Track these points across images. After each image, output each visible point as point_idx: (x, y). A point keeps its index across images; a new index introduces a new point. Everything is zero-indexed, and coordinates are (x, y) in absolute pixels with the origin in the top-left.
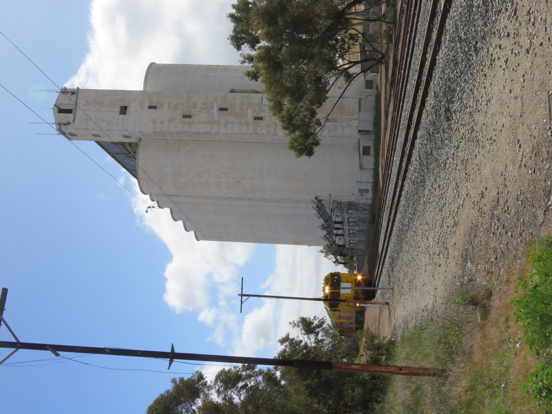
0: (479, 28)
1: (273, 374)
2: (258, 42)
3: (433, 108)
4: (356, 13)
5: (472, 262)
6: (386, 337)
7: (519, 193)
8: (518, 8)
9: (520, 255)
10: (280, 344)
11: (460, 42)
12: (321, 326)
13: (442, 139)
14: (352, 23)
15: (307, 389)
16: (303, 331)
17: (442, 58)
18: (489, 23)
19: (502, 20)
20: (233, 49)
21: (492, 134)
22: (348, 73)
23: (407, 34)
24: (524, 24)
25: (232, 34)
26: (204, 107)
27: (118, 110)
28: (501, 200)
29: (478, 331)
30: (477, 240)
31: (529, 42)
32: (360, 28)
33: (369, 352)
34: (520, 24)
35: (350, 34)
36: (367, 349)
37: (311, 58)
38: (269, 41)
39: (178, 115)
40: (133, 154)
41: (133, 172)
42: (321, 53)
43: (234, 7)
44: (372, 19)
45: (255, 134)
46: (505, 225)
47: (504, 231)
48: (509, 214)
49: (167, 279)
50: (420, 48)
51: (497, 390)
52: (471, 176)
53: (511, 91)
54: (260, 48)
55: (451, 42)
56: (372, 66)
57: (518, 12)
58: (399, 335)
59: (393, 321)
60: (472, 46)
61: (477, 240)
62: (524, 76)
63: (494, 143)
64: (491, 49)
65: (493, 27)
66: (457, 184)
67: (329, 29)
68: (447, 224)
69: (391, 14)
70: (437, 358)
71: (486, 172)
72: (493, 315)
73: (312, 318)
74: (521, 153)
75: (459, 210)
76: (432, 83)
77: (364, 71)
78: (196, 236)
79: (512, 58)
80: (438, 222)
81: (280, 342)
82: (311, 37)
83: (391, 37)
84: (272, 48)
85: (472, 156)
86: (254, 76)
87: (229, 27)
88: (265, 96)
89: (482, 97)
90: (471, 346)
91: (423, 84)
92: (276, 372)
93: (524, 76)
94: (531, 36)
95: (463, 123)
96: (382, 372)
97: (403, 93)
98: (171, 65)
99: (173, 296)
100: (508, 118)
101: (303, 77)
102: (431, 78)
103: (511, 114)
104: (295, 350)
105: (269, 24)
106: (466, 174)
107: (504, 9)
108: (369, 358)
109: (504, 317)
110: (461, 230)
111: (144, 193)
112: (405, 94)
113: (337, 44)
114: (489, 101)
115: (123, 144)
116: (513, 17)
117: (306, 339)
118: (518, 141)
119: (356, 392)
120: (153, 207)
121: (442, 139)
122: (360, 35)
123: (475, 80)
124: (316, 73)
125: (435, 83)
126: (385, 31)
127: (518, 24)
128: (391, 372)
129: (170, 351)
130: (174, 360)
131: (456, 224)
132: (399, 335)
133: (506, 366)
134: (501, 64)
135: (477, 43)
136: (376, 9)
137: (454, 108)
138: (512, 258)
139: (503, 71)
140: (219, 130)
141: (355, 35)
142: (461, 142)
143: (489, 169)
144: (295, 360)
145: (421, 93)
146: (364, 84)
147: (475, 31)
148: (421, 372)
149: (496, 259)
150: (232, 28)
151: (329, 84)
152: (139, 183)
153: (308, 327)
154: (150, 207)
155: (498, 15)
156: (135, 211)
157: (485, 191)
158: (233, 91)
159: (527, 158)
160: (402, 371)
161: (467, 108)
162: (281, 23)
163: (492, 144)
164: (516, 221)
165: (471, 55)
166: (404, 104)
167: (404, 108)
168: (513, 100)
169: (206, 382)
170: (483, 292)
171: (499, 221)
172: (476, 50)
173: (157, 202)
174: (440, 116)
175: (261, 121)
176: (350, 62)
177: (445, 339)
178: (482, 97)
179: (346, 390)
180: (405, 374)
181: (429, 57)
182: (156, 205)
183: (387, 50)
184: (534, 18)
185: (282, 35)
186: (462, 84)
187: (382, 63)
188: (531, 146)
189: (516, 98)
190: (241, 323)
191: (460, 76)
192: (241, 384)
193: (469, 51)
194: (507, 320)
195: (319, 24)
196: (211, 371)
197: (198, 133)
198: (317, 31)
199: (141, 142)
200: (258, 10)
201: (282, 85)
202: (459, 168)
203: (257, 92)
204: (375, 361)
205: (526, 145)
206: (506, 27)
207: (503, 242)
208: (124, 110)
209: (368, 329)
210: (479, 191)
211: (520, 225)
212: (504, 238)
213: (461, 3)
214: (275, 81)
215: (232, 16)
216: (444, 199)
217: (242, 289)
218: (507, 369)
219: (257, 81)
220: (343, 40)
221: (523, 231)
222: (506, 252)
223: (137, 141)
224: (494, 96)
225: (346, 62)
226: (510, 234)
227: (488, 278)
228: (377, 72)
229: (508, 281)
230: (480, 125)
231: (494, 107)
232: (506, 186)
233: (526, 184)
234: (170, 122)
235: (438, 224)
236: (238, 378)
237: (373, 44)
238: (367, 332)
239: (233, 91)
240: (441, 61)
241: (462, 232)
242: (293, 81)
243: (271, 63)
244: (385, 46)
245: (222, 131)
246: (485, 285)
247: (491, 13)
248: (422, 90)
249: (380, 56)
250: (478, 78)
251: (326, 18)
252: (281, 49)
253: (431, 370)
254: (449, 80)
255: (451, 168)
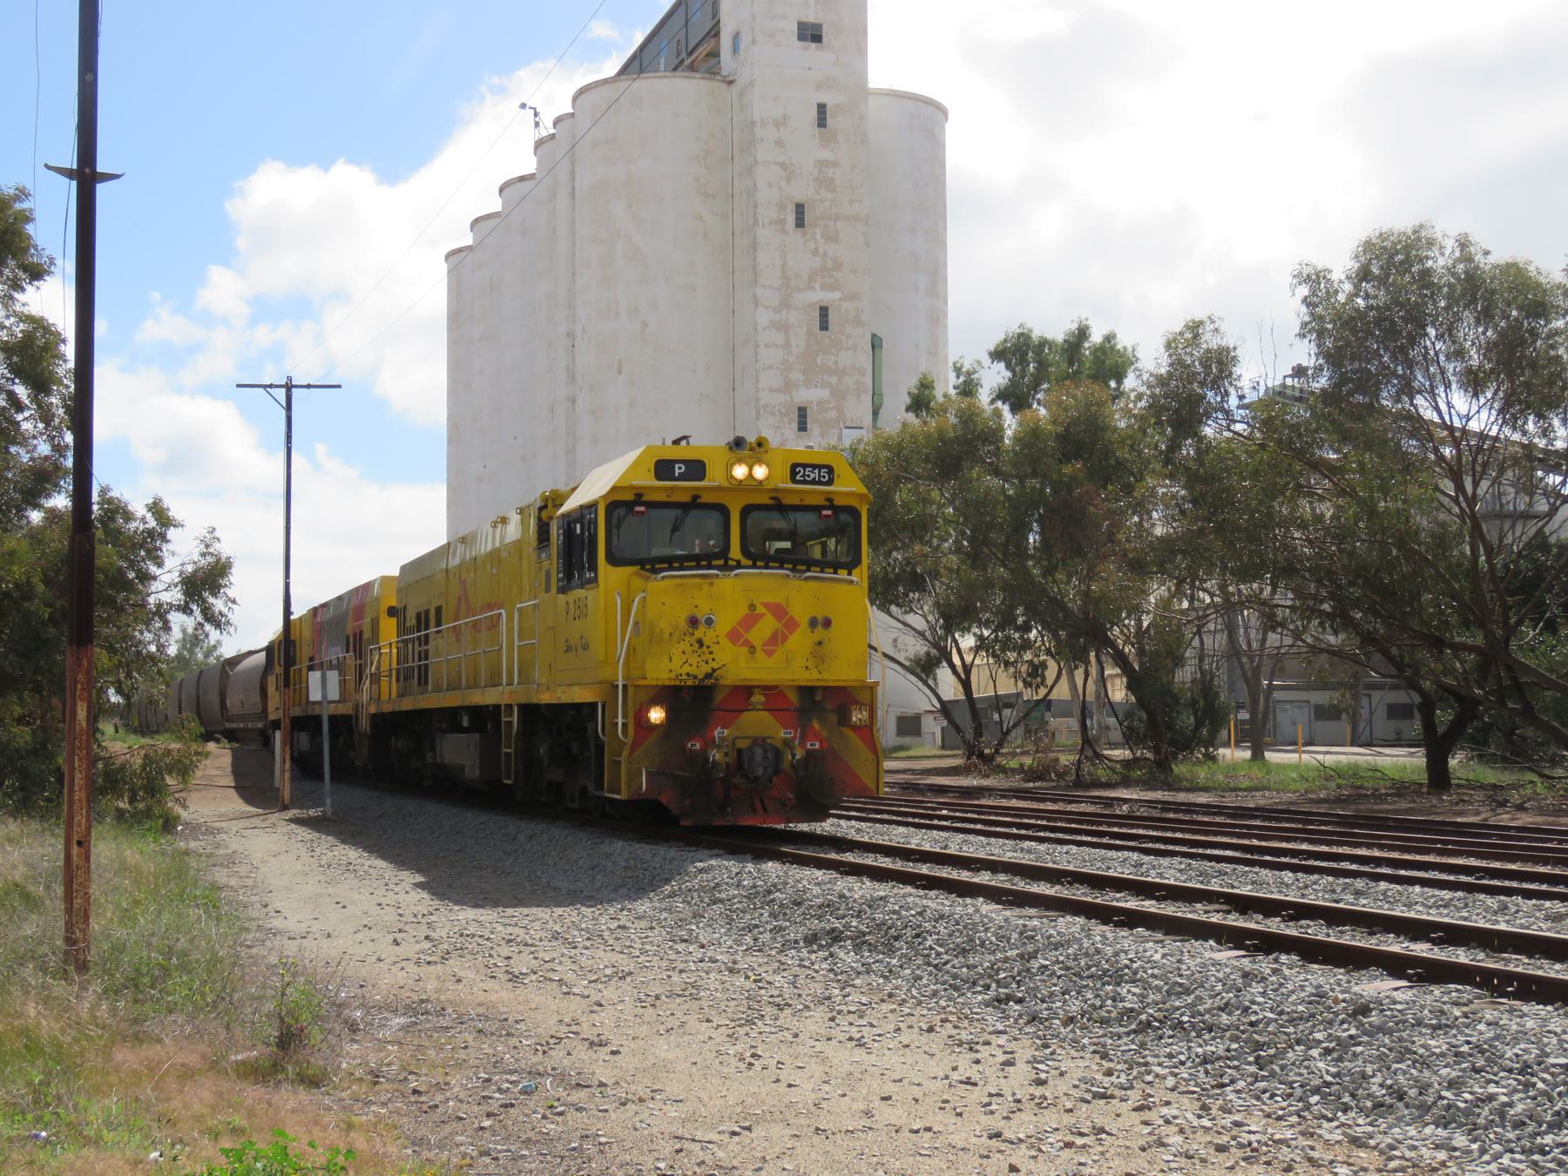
0: (1059, 1004)
1: (56, 485)
2: (1015, 409)
3: (842, 896)
4: (1102, 680)
5: (405, 1028)
6: (185, 807)
7: (603, 1140)
8: (1114, 1101)
9: (426, 1154)
10: (150, 501)
11: (1021, 956)
12: (207, 620)
13: (756, 926)
14: (1076, 667)
15: (16, 585)
16: (190, 569)
17: (977, 911)
18: (1073, 1031)
19: (1081, 1063)
20: (994, 340)
21: (769, 1055)
22: (937, 663)
23: (1049, 819)
24: (1068, 1120)
25: (1036, 335)
26: (829, 264)
27: (811, 18)
28: (582, 1094)
29: (203, 1056)
30: (470, 1038)
31: (1021, 1136)
32: (1062, 692)
33: (140, 761)
34: (1071, 1111)
35: (1043, 665)
36: (146, 755)
37: (975, 558)
38: (1017, 439)
39: (801, 191)
40: (687, 62)
41: (637, 65)
42: (989, 584)
43: (1109, 338)
44: (1088, 723)
45: (758, 411)
46: (512, 1110)
47: (494, 1106)
48: (544, 1117)
49: (326, 169)
50: (1009, 854)
51: (29, 1117)
52: (651, 1010)
53: (889, 1098)
54: (997, 414)
55: (1021, 934)
56: (958, 729)
57: (1102, 1102)
58: (193, 845)
59: (234, 826)
60: (1011, 991)
61: (470, 1038)
62: (929, 1129)
63: (742, 1066)
64: (1002, 1040)
65: (1063, 1040)
66: (630, 973)
67: (1058, 604)
68: (515, 956)
69: (1102, 773)
70: (120, 948)
71: (663, 1049)
72: (253, 1093)
73: (231, 592)
74: (714, 1137)
75: (555, 985)
76: (909, 889)
77: (946, 709)
78: (460, 250)
79: (978, 1095)
80: (522, 932)
81: (155, 503)
82: (1032, 557)
83: (1041, 778)
84: (998, 448)
85: (706, 1010)
86: (920, 402)
87: (1053, 327)
88: (866, 435)
89: (872, 1025)
90: (159, 1041)
91: (910, 867)
92: (63, 495)
93: (929, 1129)
94: (1035, 1143)
95: (801, 981)
96: (71, 791)
97: (886, 817)
98: (942, 164)
99: (275, 190)
100: (812, 1098)
101: (921, 539)
102: (924, 888)
103: (824, 1105)
104: (135, 547)
105: (1063, 438)
106: (657, 997)
107: (1111, 1065)
108: (118, 762)
109: (244, 1123)
110: (501, 995)
111: (575, 98)
112: (882, 822)
113: (1017, 629)
114: (861, 1044)
115: (714, 32)
116: (1088, 1091)
117: (167, 578)
118: (749, 1129)
119: (16, 730)
120: (537, 124)
121: (756, 926)
122: (1043, 691)
123: (920, 1003)
124: (935, 575)
125: (910, 899)
126: (1057, 760)
127: (1069, 1105)
128: (71, 816)
129: (100, 168)
130: (74, 183)
131: (515, 978)
132: (193, 845)
133: (101, 1138)
134: (961, 1069)
135: (1020, 1001)
136: (1116, 735)
137: (842, 955)
138: (419, 1134)
139: (941, 1075)
140: (767, 308)
141: (1044, 678)
142: (747, 977)
143: (670, 1056)
144: (97, 564)
145: (885, 862)
146: (910, 711)
147: (1052, 994)
148: (78, 902)
149: (415, 1092)
150: (1049, 336)
151: (906, 613)
152: (606, 81)
153: (204, 582)
154: (536, 114)
155: (1094, 1052)
156: (523, 73)
157: (608, 1049)
158: (876, 343)
159: (701, 1153)
160: (75, 850)
161: (842, 989)
162: (1067, 469)
163: (742, 1059)
164: (524, 1137)
165: (988, 987)
166: (853, 823)
167: (842, 822)
168: (862, 1107)
169: (23, 290)
170: (317, 1061)
171: (524, 1092)
172: (999, 1001)
173: (553, 136)
174: (820, 918)
175: (795, 425)
176: (967, 669)
177: (177, 968)
178: (872, 1025)
179: (21, 698)
180: (68, 858)
181: (984, 878)
182: (544, 133)
183: (1003, 770)
184: (1084, 1146)
185: (1034, 474)
186: (908, 972)
187: (969, 758)
188: (735, 1163)
189: (868, 1114)
190: (210, 390)
191: (929, 964)
192: (22, 391)
193: (998, 982)
194: (236, 1131)
195: (1070, 576)
196: (52, 301)
197: (754, 247)
198: (1049, 571)
199: (724, 86)
200: (1100, 404)
201: (897, 481)
202: (676, 978)
203: (875, 413)
204: (111, 780)
205: (737, 1149)
206: (1062, 1074)
207: (464, 1106)
208: (811, 34)
209: (207, 755)
210: (607, 1035)
211: (513, 1148)
212: (476, 1108)
213: (1126, 952)
214: (906, 460)
215: (1082, 333)
216: (588, 944)
217: (308, 386)
218: (96, 1142)
219: (908, 410)
220: (1027, 645)
221: (496, 1159)
222: (436, 1116)
223: (724, 72)
224: (873, 1058)
225: (968, 658)
226: (486, 1123)
227: (359, 1073)
228: (943, 747)
229: (350, 1126)
230: (794, 1024)
231: (844, 1057)
232: (623, 1104)
233: (628, 1158)
234: (783, 165)
235: (516, 930)
236: (41, 384)
237: (1020, 730)
238: (197, 753)
239: (876, 343)
240: (971, 910)
241: (494, 997)
242: (910, 511)
243: (957, 448)
244: (1013, 764)
245: (763, 317)
246: (339, 1067)
247: (1101, 1032)
248: (891, 866)
249: (987, 751)
250: (925, 1012)
251: (1086, 595)
252: (997, 472)
253: (83, 931)
254: (918, 936)
255: (674, 957)
